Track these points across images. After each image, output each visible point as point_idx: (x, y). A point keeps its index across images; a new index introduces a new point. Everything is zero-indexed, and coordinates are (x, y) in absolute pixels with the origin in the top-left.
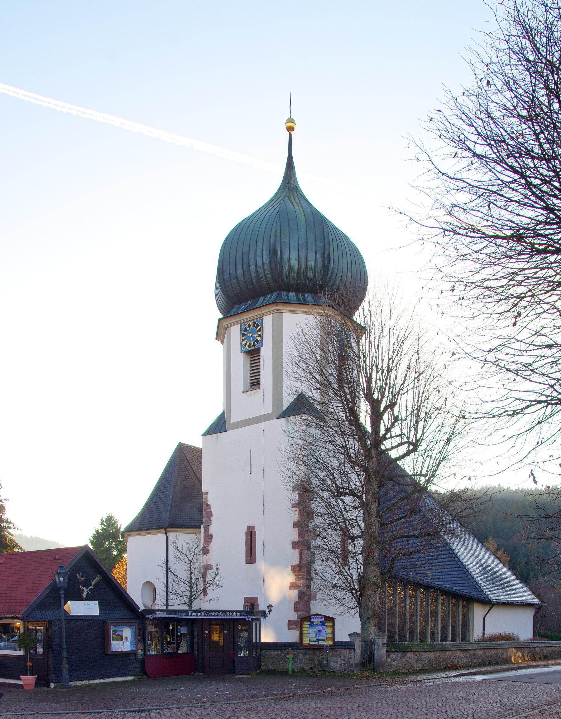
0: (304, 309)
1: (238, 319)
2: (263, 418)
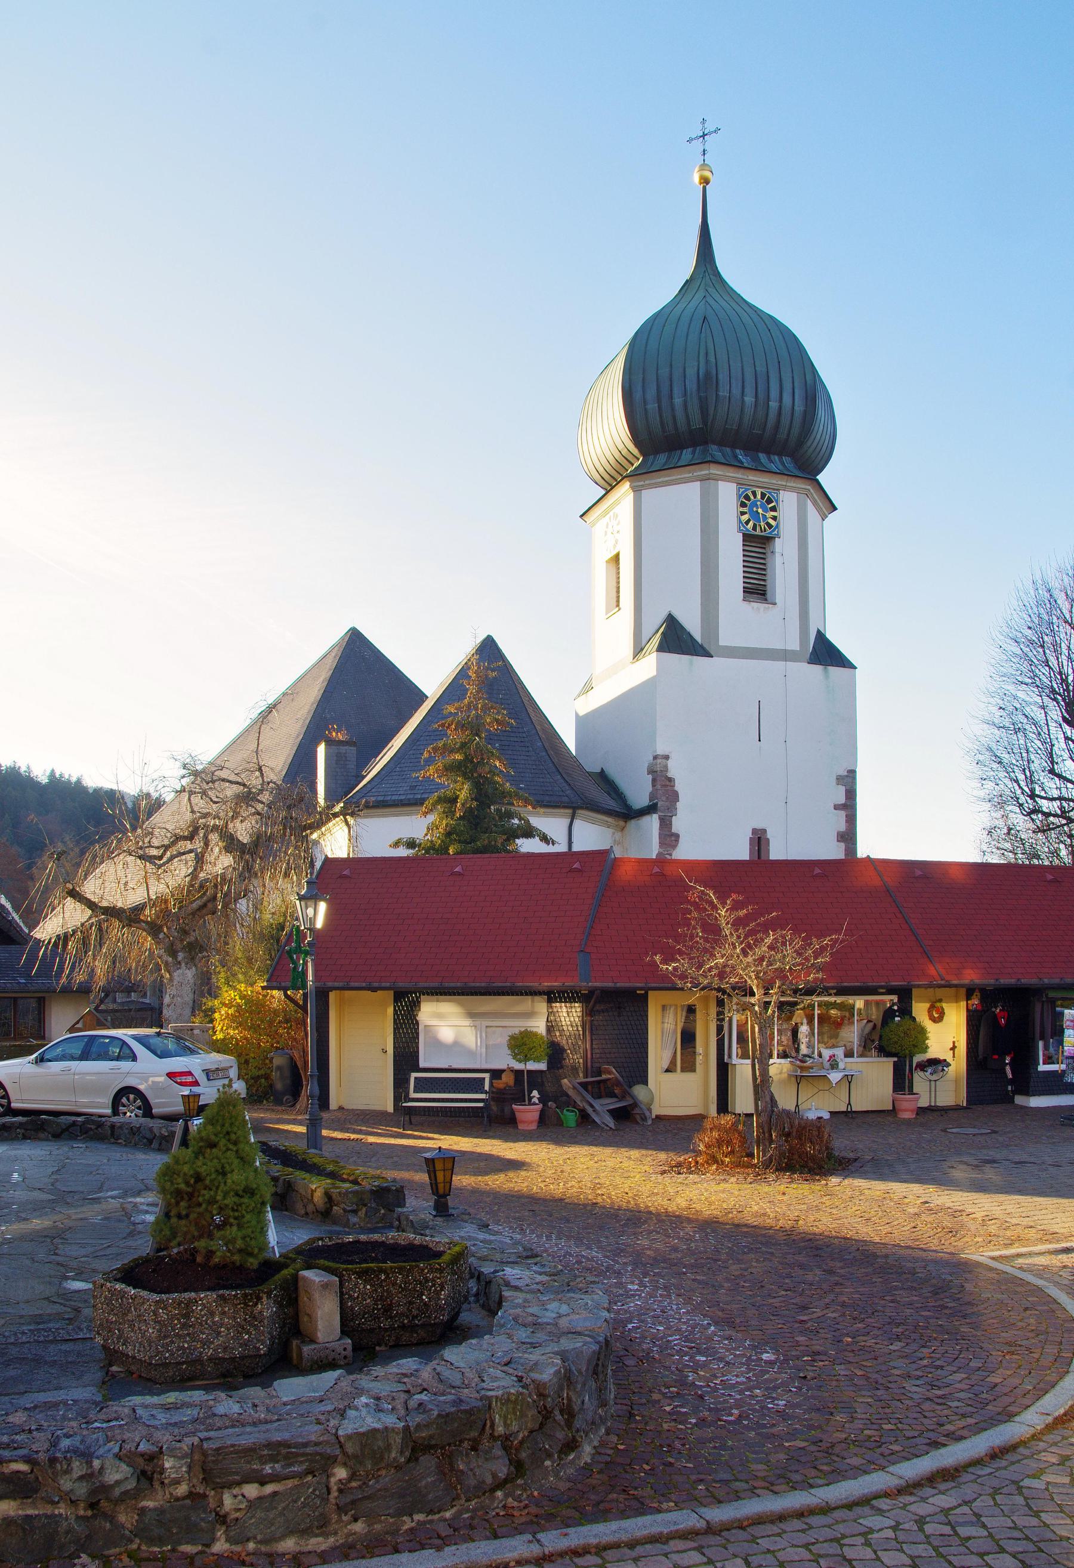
0: (676, 475)
1: (740, 476)
2: (785, 656)
